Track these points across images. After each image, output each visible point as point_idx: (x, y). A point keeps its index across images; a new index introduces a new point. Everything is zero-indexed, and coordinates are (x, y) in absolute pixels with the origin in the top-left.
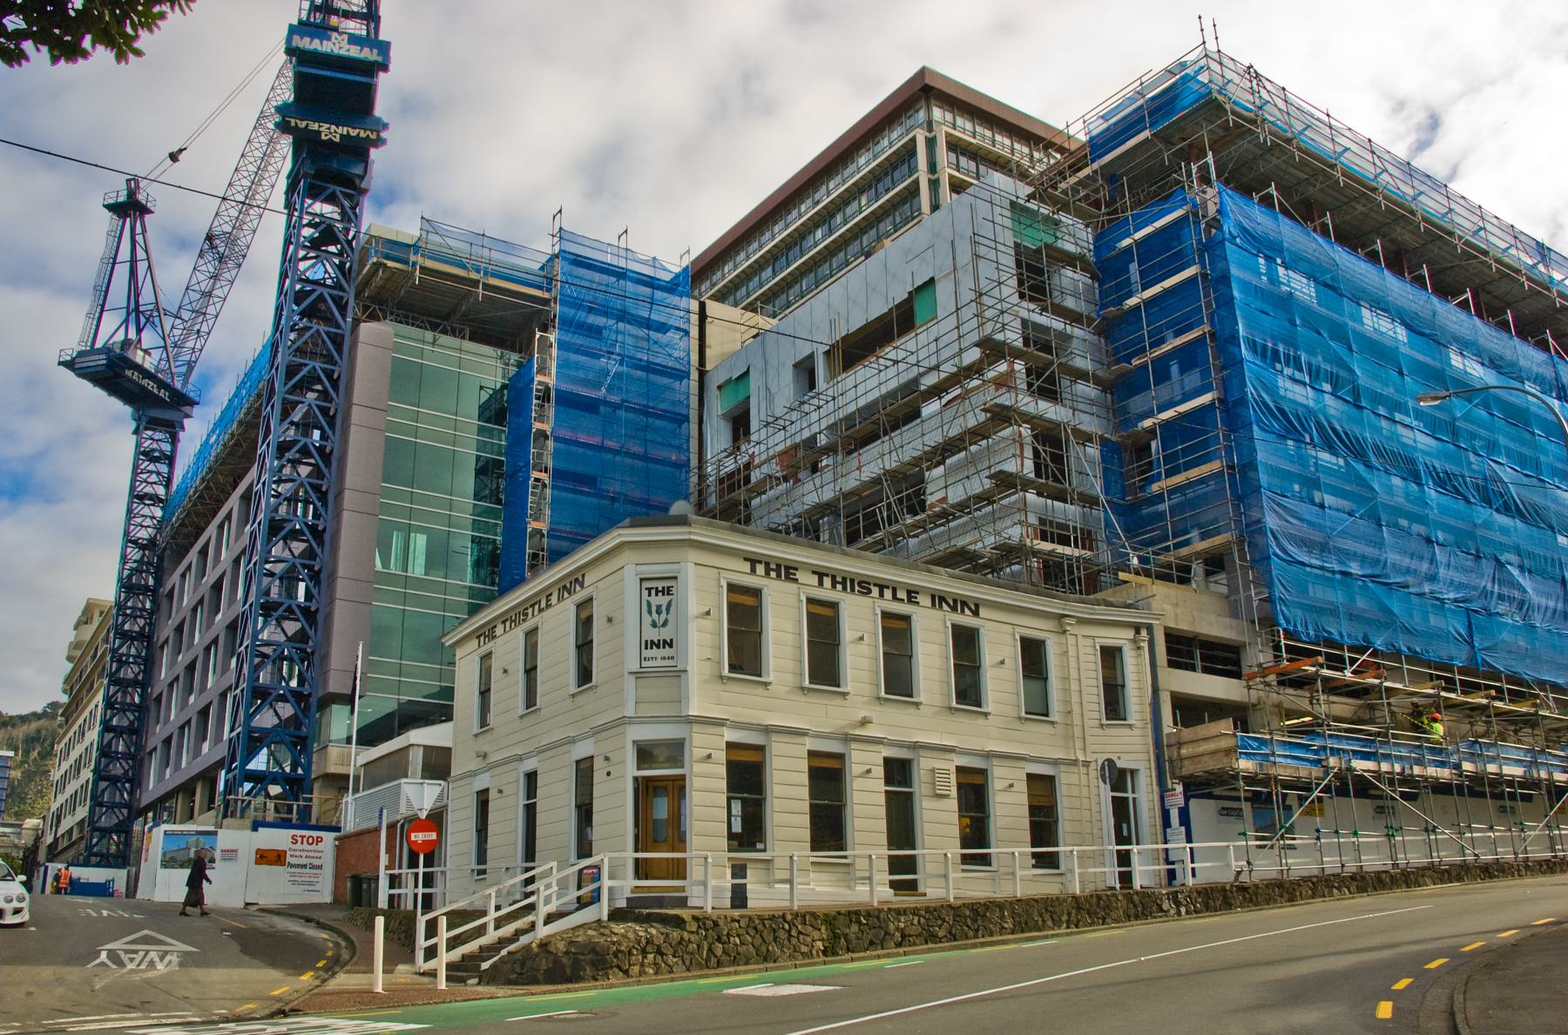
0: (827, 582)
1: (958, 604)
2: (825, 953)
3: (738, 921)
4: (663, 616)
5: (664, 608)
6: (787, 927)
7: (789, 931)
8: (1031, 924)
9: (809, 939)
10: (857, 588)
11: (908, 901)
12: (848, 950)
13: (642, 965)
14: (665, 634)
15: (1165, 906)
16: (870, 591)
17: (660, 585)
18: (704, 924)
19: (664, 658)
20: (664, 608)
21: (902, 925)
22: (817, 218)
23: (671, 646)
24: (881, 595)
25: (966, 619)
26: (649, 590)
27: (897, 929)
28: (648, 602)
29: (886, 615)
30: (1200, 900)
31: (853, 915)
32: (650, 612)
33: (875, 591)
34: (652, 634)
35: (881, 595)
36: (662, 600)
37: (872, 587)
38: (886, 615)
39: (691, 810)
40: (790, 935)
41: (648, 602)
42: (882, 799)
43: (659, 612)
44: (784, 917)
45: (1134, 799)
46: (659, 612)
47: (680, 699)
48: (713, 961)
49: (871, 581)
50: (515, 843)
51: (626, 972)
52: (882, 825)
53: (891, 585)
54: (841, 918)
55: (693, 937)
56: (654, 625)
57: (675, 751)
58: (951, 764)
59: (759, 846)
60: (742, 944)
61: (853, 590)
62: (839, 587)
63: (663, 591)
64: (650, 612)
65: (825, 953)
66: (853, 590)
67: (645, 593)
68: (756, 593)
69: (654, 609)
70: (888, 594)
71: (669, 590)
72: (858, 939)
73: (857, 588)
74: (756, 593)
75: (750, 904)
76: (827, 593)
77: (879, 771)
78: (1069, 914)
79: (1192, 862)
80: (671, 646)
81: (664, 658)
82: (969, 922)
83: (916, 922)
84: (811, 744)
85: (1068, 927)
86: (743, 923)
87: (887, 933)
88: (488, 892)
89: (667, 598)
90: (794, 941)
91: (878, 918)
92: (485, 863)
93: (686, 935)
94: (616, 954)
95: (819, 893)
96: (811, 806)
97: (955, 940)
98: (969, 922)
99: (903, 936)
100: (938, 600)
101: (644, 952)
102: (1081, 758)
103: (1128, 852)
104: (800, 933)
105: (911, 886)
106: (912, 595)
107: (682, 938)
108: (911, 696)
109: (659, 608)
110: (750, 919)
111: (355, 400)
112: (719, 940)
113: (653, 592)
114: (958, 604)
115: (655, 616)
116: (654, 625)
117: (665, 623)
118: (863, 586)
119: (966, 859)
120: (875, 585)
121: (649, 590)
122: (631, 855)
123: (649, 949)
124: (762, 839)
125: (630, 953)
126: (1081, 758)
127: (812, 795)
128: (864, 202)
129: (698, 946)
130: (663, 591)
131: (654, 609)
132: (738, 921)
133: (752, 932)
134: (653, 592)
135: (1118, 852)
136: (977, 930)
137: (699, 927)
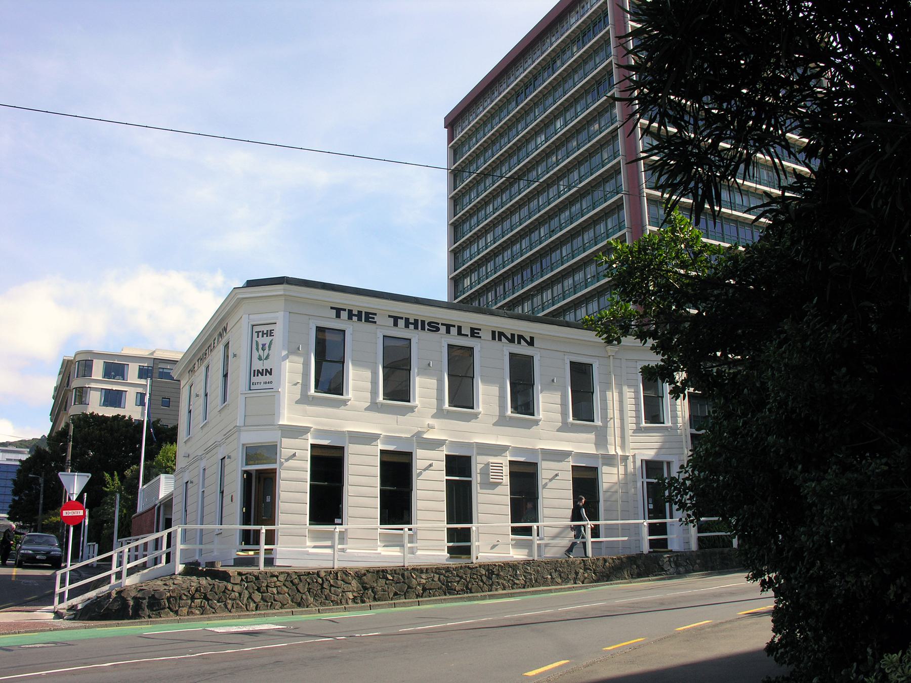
0: (401, 323)
2: (354, 600)
3: (277, 577)
4: (266, 351)
5: (267, 346)
6: (320, 580)
7: (322, 585)
8: (540, 580)
9: (340, 590)
10: (427, 327)
11: (461, 561)
12: (375, 599)
13: (190, 607)
14: (267, 365)
16: (438, 329)
17: (265, 329)
18: (247, 578)
19: (265, 383)
20: (267, 346)
21: (424, 581)
22: (544, 63)
23: (271, 374)
24: (448, 332)
25: (522, 349)
26: (258, 332)
27: (419, 584)
28: (257, 342)
30: (698, 561)
31: (381, 573)
32: (258, 350)
33: (443, 329)
34: (258, 365)
35: (448, 332)
36: (266, 340)
37: (440, 326)
39: (279, 496)
40: (322, 588)
41: (257, 342)
42: (444, 486)
43: (263, 349)
44: (318, 574)
46: (263, 349)
47: (273, 412)
48: (252, 605)
49: (440, 322)
51: (176, 613)
52: (443, 506)
53: (347, 308)
54: (369, 575)
55: (237, 588)
56: (260, 359)
57: (271, 451)
58: (504, 461)
59: (337, 521)
60: (278, 593)
62: (411, 327)
63: (267, 334)
64: (258, 350)
65: (354, 600)
67: (255, 335)
69: (260, 347)
70: (454, 331)
71: (271, 333)
72: (384, 591)
75: (278, 562)
76: (401, 332)
77: (443, 465)
78: (577, 573)
80: (271, 374)
81: (265, 383)
82: (484, 578)
83: (436, 579)
84: (381, 446)
85: (575, 583)
86: (281, 578)
87: (409, 587)
89: (270, 338)
90: (327, 592)
91: (403, 575)
93: (230, 586)
94: (168, 599)
95: (384, 556)
96: (312, 487)
97: (471, 592)
98: (484, 578)
99: (424, 589)
100: (497, 335)
101: (193, 598)
102: (620, 453)
104: (331, 586)
105: (467, 551)
106: (474, 333)
107: (226, 588)
108: (533, 414)
109: (264, 345)
110: (288, 574)
112: (259, 590)
113: (261, 334)
115: (261, 351)
116: (260, 359)
117: (267, 358)
119: (515, 531)
120: (442, 324)
123: (197, 595)
124: (340, 516)
125: (181, 598)
126: (620, 453)
127: (313, 477)
128: (575, 50)
129: (240, 594)
130: (267, 334)
131: (260, 347)
132: (277, 577)
133: (288, 584)
134: (261, 334)
136: (491, 585)
137: (242, 580)
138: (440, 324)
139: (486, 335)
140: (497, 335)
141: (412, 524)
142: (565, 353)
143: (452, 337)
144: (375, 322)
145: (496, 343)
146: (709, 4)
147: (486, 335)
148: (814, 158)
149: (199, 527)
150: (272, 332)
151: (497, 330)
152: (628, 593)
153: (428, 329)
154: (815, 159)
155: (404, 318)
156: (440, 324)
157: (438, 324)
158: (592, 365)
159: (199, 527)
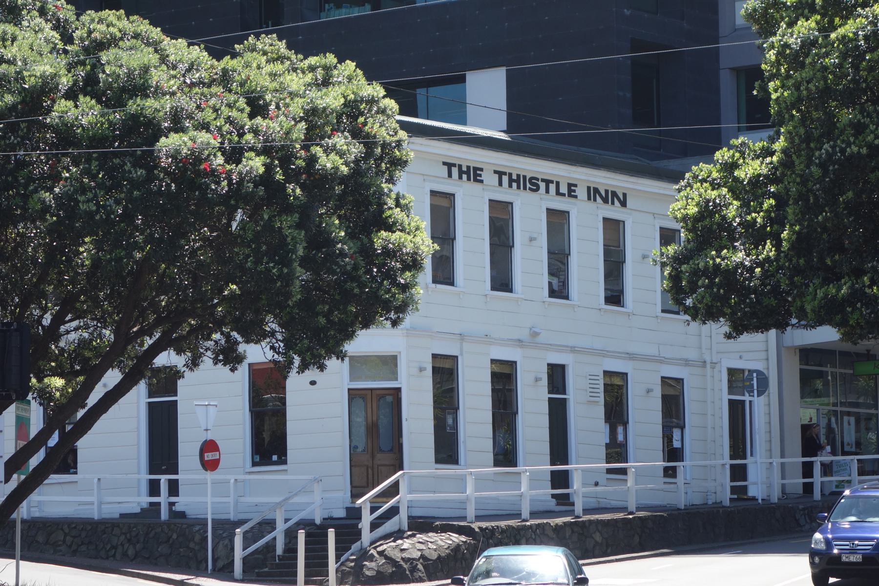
1: (610, 197)
10: (528, 185)
15: (802, 522)
16: (538, 189)
26: (450, 166)
29: (550, 212)
33: (542, 185)
38: (550, 212)
45: (750, 402)
49: (540, 177)
50: (138, 428)
61: (525, 188)
66: (525, 188)
68: (451, 197)
73: (528, 185)
74: (451, 197)
76: (504, 194)
79: (783, 478)
88: (228, 477)
92: (566, 462)
100: (593, 193)
103: (812, 463)
111: (431, 89)
114: (610, 197)
118: (532, 184)
121: (450, 166)
122: (728, 462)
135: (804, 463)
138: (540, 180)
139: (581, 192)
140: (593, 193)
141: (683, 461)
142: (425, 177)
143: (629, 211)
144: (482, 181)
145: (591, 205)
146: (94, 152)
147: (581, 192)
148: (111, 369)
149: (760, 485)
150: (478, 172)
151: (592, 186)
152: (604, 503)
153: (530, 189)
154: (112, 370)
155: (555, 182)
156: (540, 180)
157: (537, 179)
158: (512, 204)
159: (760, 485)
